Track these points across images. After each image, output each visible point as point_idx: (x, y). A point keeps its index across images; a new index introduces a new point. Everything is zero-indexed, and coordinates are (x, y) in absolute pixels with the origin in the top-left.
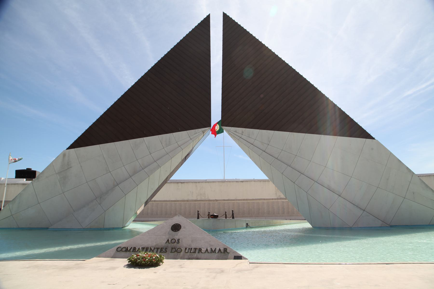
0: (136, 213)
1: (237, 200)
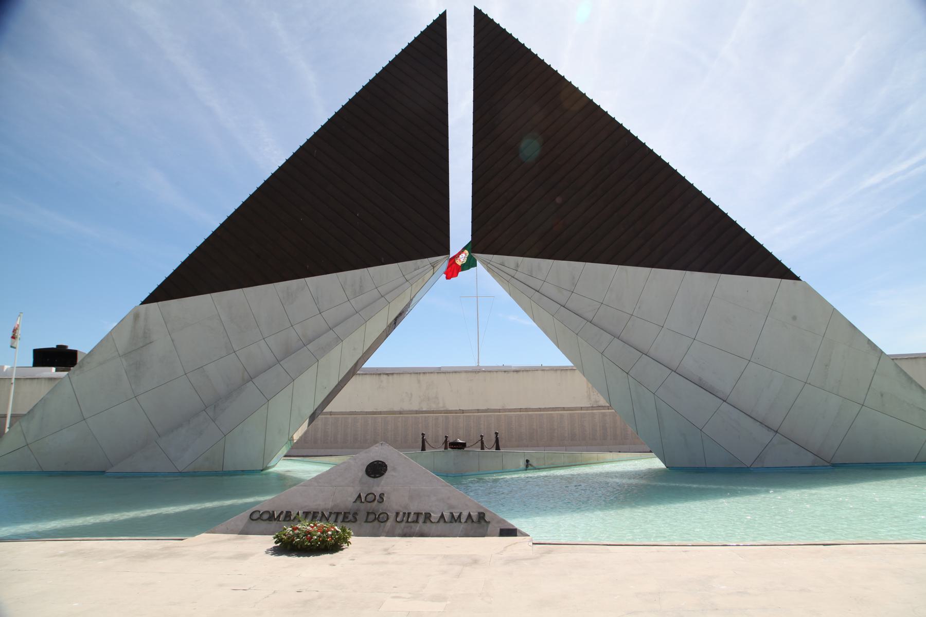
0: (291, 439)
1: (505, 410)
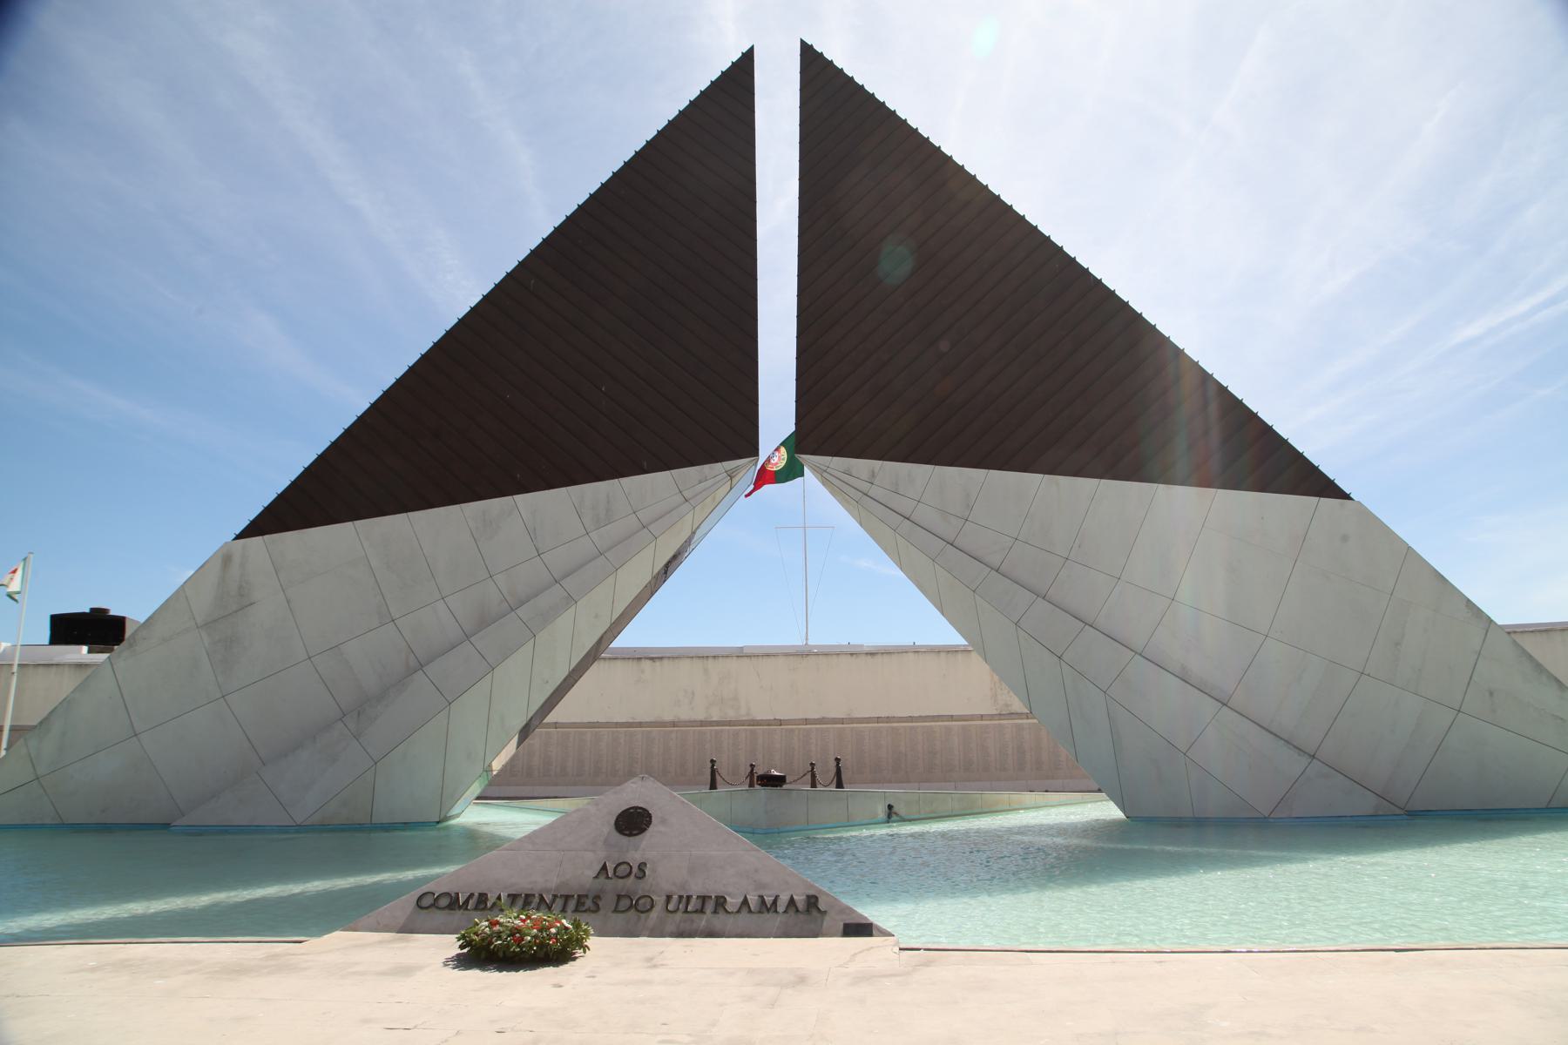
0: (489, 769)
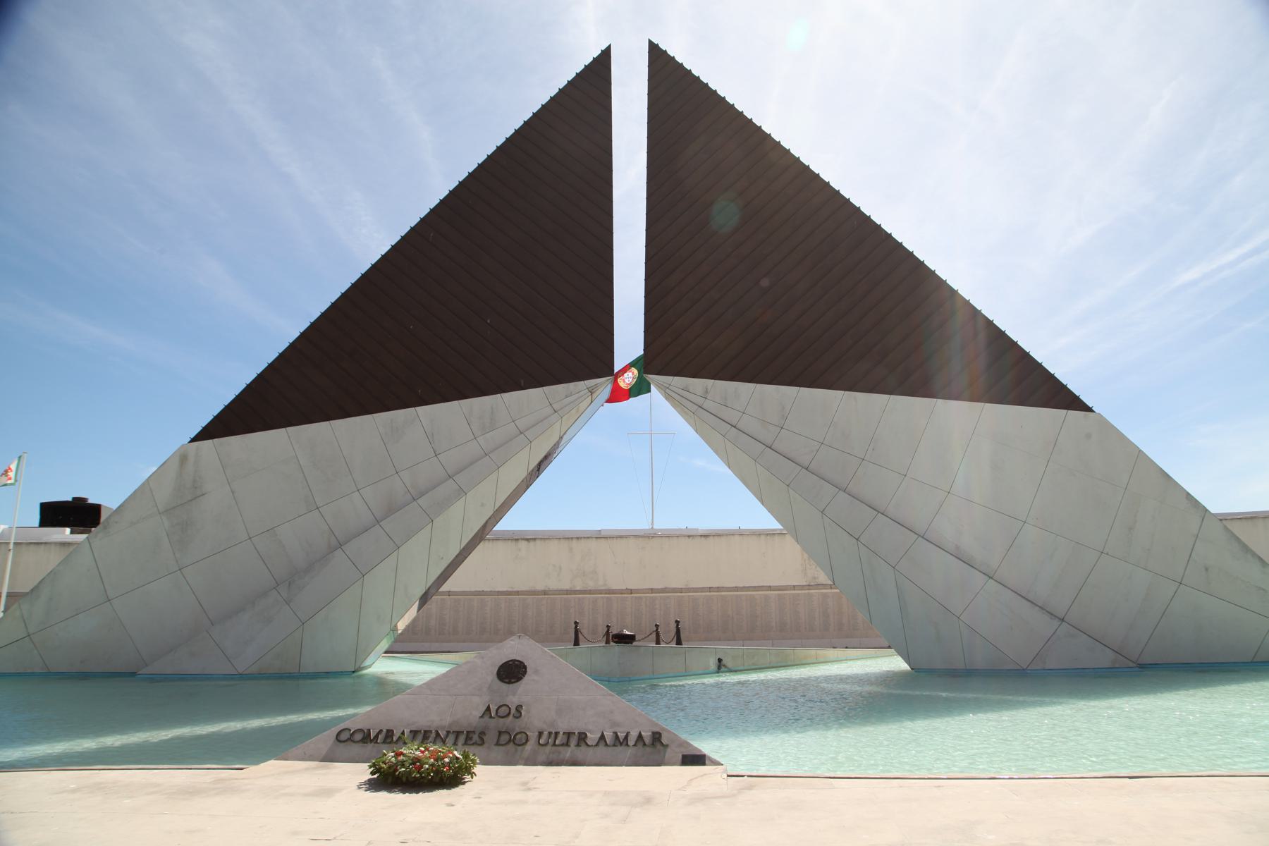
0: (395, 629)
